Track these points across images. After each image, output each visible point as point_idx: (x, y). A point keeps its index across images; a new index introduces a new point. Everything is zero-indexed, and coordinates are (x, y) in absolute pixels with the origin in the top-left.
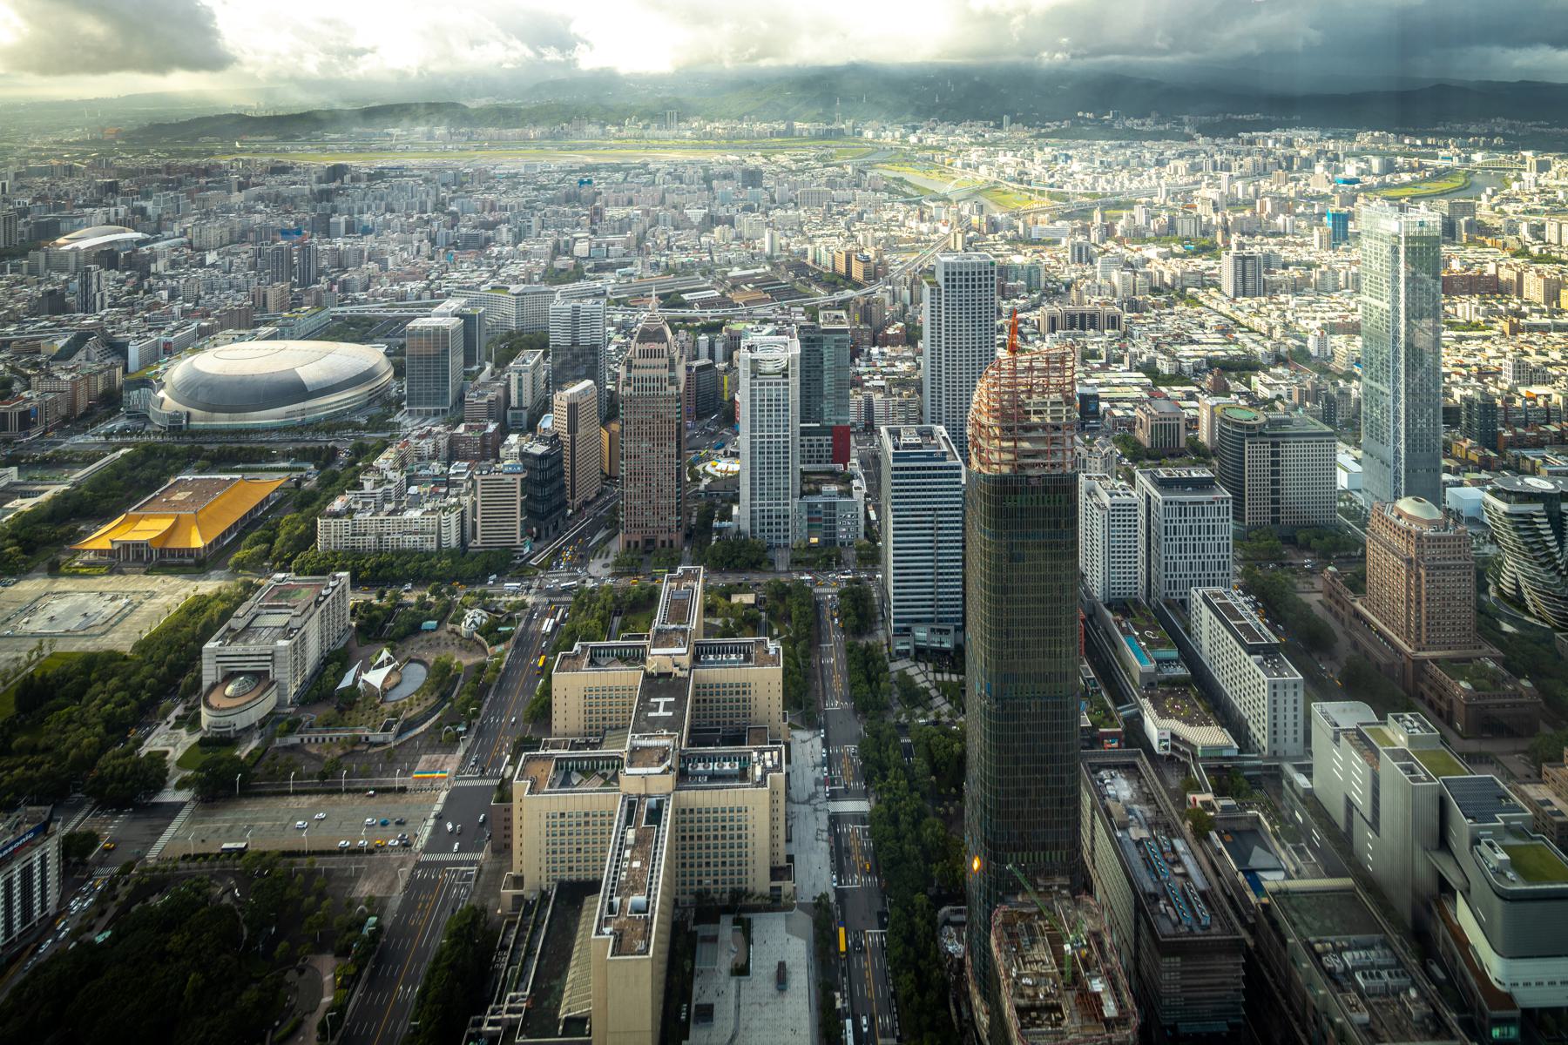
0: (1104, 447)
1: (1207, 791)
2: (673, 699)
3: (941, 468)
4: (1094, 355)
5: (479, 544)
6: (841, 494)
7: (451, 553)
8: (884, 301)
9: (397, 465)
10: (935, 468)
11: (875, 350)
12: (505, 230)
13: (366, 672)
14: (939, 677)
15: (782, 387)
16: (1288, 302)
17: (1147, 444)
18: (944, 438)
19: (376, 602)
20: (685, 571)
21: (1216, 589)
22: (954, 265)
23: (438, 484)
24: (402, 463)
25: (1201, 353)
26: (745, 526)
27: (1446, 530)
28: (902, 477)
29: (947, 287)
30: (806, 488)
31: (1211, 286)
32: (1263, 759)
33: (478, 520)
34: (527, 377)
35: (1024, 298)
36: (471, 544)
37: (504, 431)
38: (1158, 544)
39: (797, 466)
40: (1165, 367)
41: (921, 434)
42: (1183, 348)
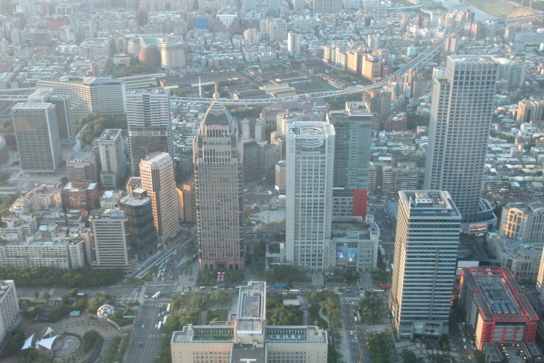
2: (255, 360)
5: (99, 264)
6: (362, 237)
7: (79, 270)
9: (27, 211)
12: (67, 30)
13: (40, 340)
14: (430, 352)
15: (320, 160)
19: (32, 299)
20: (253, 284)
22: (463, 65)
23: (60, 225)
24: (30, 209)
26: (290, 256)
29: (455, 84)
30: (337, 232)
33: (97, 249)
34: (112, 150)
35: (505, 94)
36: (93, 264)
37: (101, 189)
39: (328, 217)
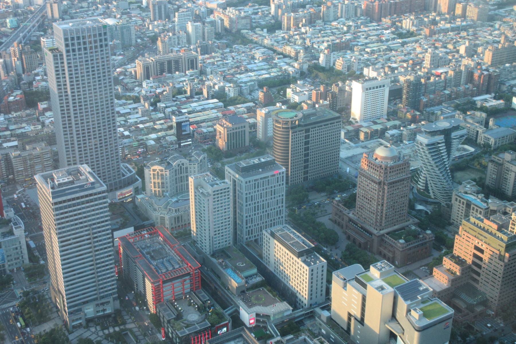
0: (199, 156)
1: (277, 335)
10: (73, 199)
14: (106, 332)
16: (306, 33)
18: (89, 173)
22: (71, 31)
25: (254, 78)
27: (399, 161)
28: (61, 208)
29: (68, 51)
31: (257, 27)
32: (305, 310)
35: (120, 55)
38: (241, 210)
40: (231, 91)
41: (70, 174)
42: (242, 76)
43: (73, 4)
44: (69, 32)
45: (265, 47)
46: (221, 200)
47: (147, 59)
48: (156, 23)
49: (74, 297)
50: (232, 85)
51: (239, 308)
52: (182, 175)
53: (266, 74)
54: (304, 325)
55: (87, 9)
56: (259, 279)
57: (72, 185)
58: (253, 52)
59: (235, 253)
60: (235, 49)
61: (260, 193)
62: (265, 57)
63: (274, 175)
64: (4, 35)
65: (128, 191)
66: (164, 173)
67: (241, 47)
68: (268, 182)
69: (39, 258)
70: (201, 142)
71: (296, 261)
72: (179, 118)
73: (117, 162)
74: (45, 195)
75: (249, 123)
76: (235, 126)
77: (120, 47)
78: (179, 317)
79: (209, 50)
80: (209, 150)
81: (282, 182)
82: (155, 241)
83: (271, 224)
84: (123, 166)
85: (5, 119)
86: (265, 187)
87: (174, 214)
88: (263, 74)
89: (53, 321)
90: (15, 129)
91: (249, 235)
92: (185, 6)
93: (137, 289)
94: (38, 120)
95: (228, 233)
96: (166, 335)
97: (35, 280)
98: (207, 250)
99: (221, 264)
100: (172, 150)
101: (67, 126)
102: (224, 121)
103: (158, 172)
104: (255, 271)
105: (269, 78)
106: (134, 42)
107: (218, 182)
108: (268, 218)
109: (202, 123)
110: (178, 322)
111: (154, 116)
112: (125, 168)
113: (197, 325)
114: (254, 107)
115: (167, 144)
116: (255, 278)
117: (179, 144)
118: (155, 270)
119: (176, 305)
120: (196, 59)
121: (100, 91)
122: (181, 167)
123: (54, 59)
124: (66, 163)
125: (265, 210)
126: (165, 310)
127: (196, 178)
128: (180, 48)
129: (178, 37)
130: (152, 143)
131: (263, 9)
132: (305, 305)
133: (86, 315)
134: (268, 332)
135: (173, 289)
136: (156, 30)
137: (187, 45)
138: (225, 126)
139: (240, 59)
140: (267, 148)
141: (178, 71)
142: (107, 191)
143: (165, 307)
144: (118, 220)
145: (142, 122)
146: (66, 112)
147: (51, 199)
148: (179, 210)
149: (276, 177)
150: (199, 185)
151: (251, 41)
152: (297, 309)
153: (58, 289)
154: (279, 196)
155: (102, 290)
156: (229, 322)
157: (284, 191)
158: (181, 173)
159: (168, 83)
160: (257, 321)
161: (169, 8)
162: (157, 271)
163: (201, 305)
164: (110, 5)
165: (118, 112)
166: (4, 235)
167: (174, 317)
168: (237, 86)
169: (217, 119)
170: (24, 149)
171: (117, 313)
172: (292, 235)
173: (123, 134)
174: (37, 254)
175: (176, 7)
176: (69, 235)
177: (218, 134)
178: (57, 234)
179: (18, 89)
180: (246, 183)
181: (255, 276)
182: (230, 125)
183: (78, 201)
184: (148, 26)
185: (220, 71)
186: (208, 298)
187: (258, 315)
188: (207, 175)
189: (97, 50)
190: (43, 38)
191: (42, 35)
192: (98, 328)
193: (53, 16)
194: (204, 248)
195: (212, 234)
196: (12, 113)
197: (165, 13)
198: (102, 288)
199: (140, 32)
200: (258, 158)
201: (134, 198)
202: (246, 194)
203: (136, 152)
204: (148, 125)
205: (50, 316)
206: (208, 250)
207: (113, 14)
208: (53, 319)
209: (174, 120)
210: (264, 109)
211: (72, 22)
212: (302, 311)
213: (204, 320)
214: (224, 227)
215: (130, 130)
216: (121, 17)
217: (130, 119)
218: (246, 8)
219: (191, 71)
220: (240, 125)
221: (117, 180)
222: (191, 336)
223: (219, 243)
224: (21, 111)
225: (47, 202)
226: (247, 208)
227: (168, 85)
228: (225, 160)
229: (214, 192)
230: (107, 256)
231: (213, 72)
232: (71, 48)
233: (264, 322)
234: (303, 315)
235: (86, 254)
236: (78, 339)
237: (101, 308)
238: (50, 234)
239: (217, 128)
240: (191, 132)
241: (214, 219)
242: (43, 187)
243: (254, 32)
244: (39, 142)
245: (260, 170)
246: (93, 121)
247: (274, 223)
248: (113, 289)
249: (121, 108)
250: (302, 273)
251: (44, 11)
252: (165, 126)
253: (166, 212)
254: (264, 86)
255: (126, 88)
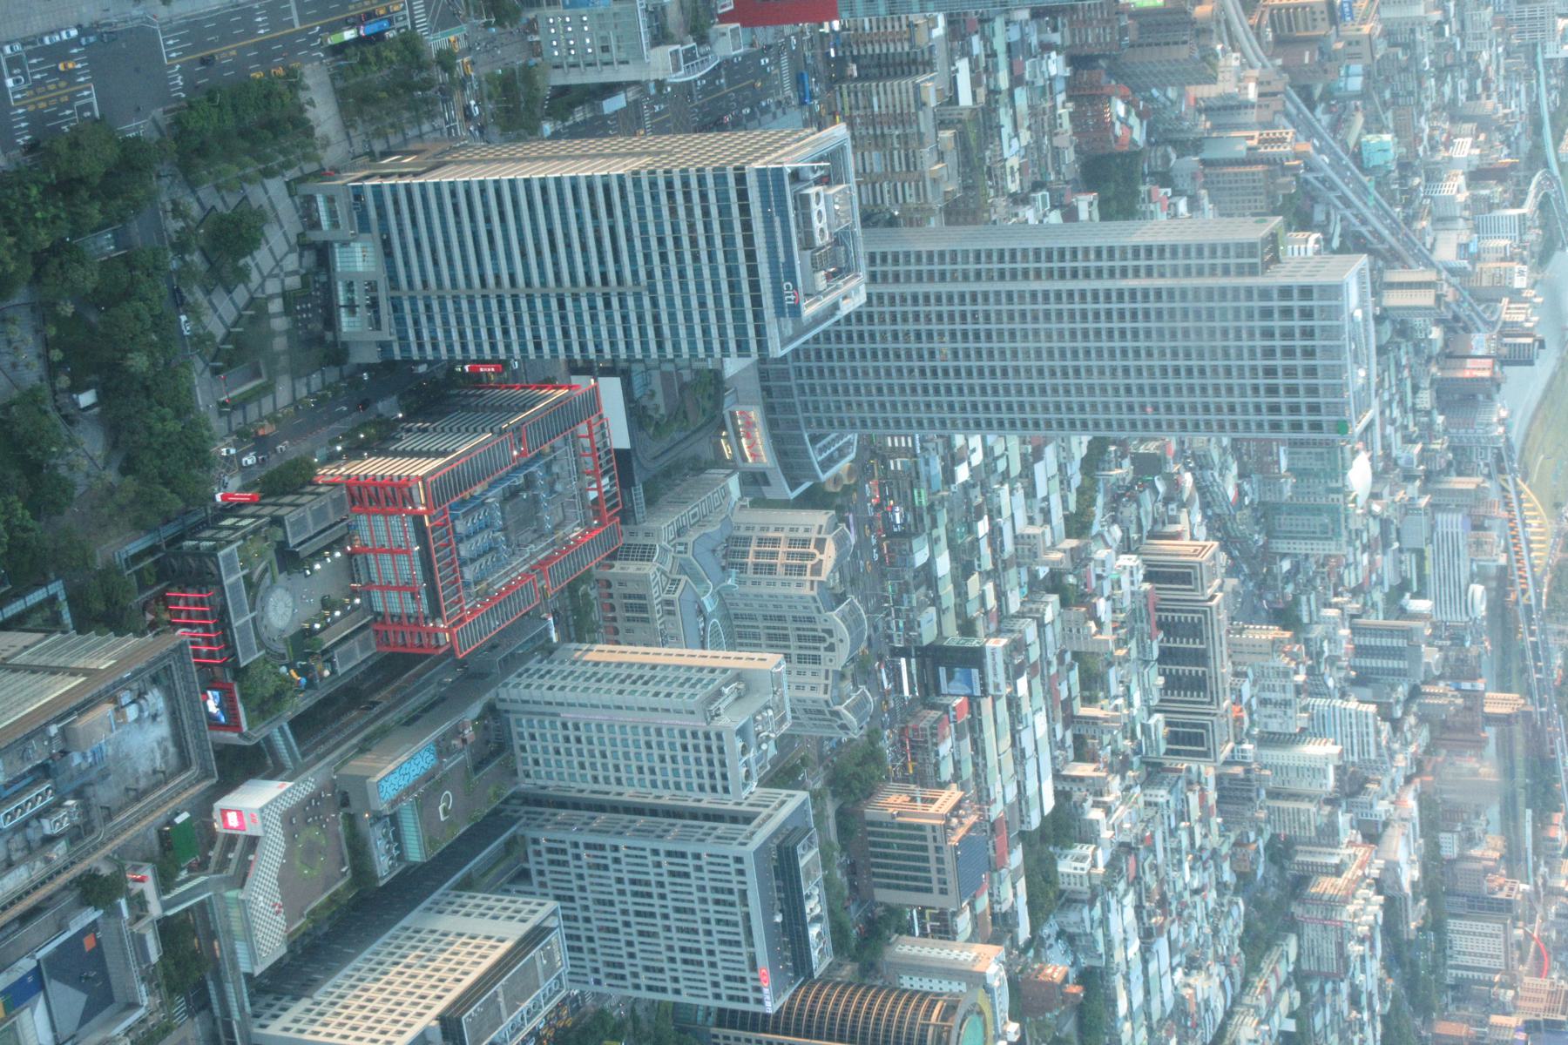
1: (166, 906)
3: (758, 316)
4: (1093, 684)
8: (1213, 80)
11: (1055, 65)
14: (276, 306)
17: (870, 812)
18: (835, 307)
21: (562, 959)
25: (1119, 956)
28: (723, 197)
29: (1265, 293)
31: (1305, 997)
35: (1241, 493)
38: (643, 832)
40: (1075, 865)
41: (838, 240)
42: (1130, 913)
43: (1430, 359)
44: (1334, 303)
45: (1229, 1014)
46: (686, 760)
47: (1217, 582)
48: (1345, 632)
49: (412, 211)
50: (1101, 869)
51: (290, 779)
52: (793, 643)
53: (1130, 1003)
54: (191, 1014)
55: (1409, 404)
56: (383, 865)
57: (800, 240)
58: (1216, 969)
59: (491, 791)
60: (1231, 903)
61: (697, 906)
62: (1192, 1009)
63: (754, 967)
64: (1339, 119)
65: (757, 448)
66: (808, 577)
67: (1236, 926)
68: (730, 943)
69: (564, 120)
70: (903, 730)
71: (428, 1007)
72: (1000, 659)
73: (864, 423)
74: (776, 150)
75: (954, 914)
76: (948, 856)
77: (1269, 498)
78: (289, 560)
79: (1231, 808)
80: (871, 756)
81: (724, 993)
82: (570, 512)
83: (578, 938)
84: (849, 443)
85: (1051, 79)
86: (714, 927)
87: (656, 595)
88: (1129, 993)
89: (341, 136)
90: (1013, 106)
91: (550, 850)
92: (1396, 746)
93: (409, 430)
94: (1037, 186)
95: (565, 771)
96: (232, 509)
97: (490, 97)
98: (515, 690)
99: (457, 732)
100: (888, 623)
101: (1007, 266)
102: (973, 819)
103: (813, 556)
104: (415, 854)
105: (1114, 1013)
106: (1281, 546)
107: (752, 755)
108: (600, 929)
109: (974, 742)
110: (271, 555)
111: (1015, 580)
112: (839, 450)
113: (249, 616)
114: (1014, 940)
115: (911, 609)
116: (388, 851)
117: (904, 652)
118: (466, 494)
119: (331, 555)
120: (1205, 755)
121: (1116, 390)
122: (822, 640)
123: (1240, 246)
124: (878, 249)
125: (632, 919)
126: (320, 514)
127: (776, 680)
128: (1249, 705)
129: (1286, 704)
130: (920, 558)
131: (1368, 1030)
132: (263, 1026)
133: (345, 244)
134: (184, 874)
135: (391, 552)
136: (1317, 631)
137: (1256, 731)
138: (955, 821)
139: (1191, 917)
140: (856, 966)
141: (1167, 688)
142: (763, 359)
143: (332, 518)
144: (659, 399)
145: (995, 533)
146: (1056, 265)
147: (758, 165)
148: (671, 613)
149: (748, 975)
150: (748, 689)
151: (1253, 967)
152: (251, 995)
153: (445, 164)
154: (676, 980)
155: (421, 307)
156: (242, 735)
157: (694, 1001)
158: (800, 638)
159: (1126, 643)
160: (231, 840)
161: (1393, 688)
162: (463, 502)
163: (321, 643)
164: (1418, 483)
165: (1038, 455)
166: (656, 15)
167: (292, 542)
168: (1093, 888)
169: (980, 800)
170: (942, 124)
171: (337, 354)
172: (528, 1004)
173: (961, 461)
174: (579, 115)
175: (1398, 712)
176: (626, 215)
177: (928, 793)
178: (636, 173)
179: (1149, 134)
180: (739, 860)
181: (395, 853)
182: (954, 840)
183: (749, 316)
184: (1336, 606)
185: (1152, 836)
186: (340, 671)
187: (252, 842)
188: (783, 720)
189: (1262, 392)
190: (1317, 241)
191: (1328, 241)
192: (293, 282)
193: (1391, 286)
194: (525, 680)
195: (568, 715)
196: (1070, 105)
197: (1377, 670)
198: (428, 307)
199: (1316, 573)
200: (825, 914)
201: (732, 466)
202: (697, 856)
203: (891, 497)
204: (985, 550)
205: (360, 128)
206: (514, 694)
207: (1386, 492)
208: (348, 134)
209: (991, 643)
210: (1003, 973)
211: (1365, 320)
212: (242, 1009)
213: (262, 645)
214: (587, 760)
215: (974, 486)
216: (1375, 517)
217: (1011, 493)
218: (1374, 966)
219: (1163, 731)
220: (951, 878)
221: (801, 416)
222: (214, 590)
223: (533, 737)
224: (1075, 134)
225: (749, 153)
226: (647, 853)
227: (1120, 643)
228: (831, 809)
229: (719, 736)
230: (536, 337)
231: (1151, 812)
232: (1276, 304)
233: (223, 863)
234: (227, 1013)
235: (556, 264)
236: (267, 207)
237: (361, 298)
238: (639, 155)
239: (946, 793)
240: (945, 701)
241: (622, 727)
242: (802, 147)
243: (1287, 984)
244: (964, 176)
245: (779, 919)
246: (1015, 353)
247: (580, 949)
248: (421, 346)
249: (1054, 469)
250: (380, 1027)
251: (1411, 262)
252: (973, 610)
253: (667, 568)
254: (1087, 989)
255: (1116, 499)
